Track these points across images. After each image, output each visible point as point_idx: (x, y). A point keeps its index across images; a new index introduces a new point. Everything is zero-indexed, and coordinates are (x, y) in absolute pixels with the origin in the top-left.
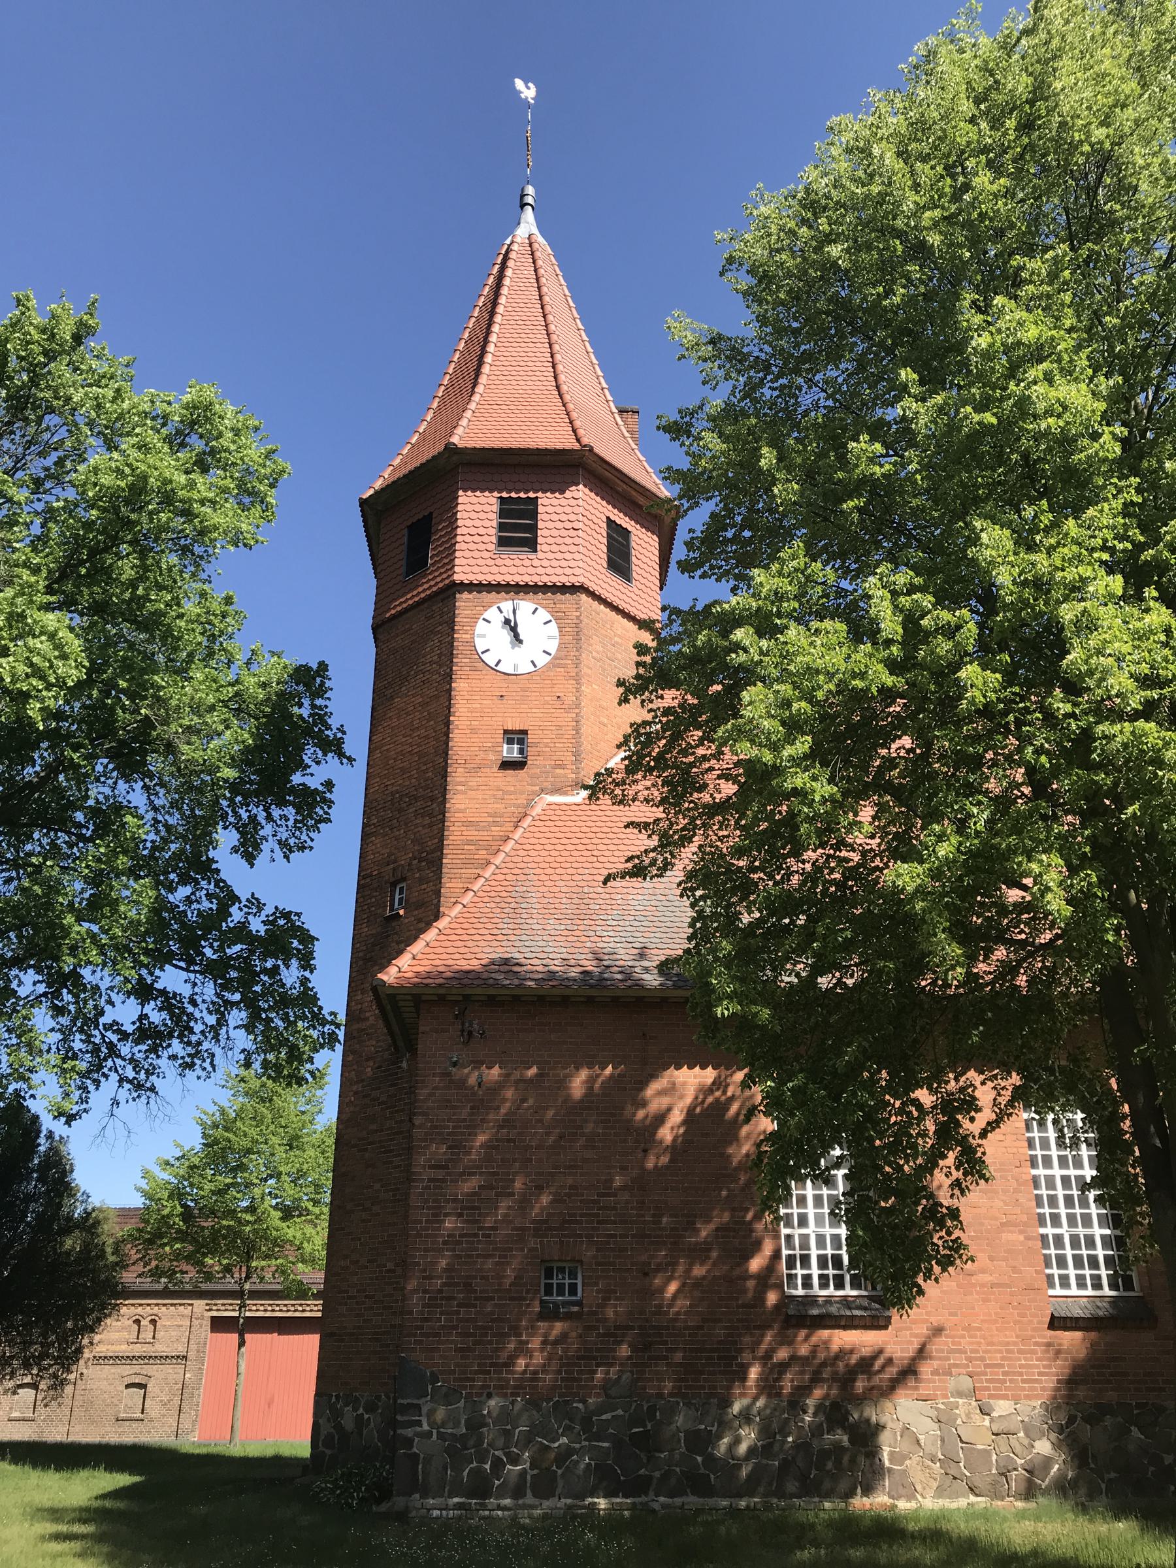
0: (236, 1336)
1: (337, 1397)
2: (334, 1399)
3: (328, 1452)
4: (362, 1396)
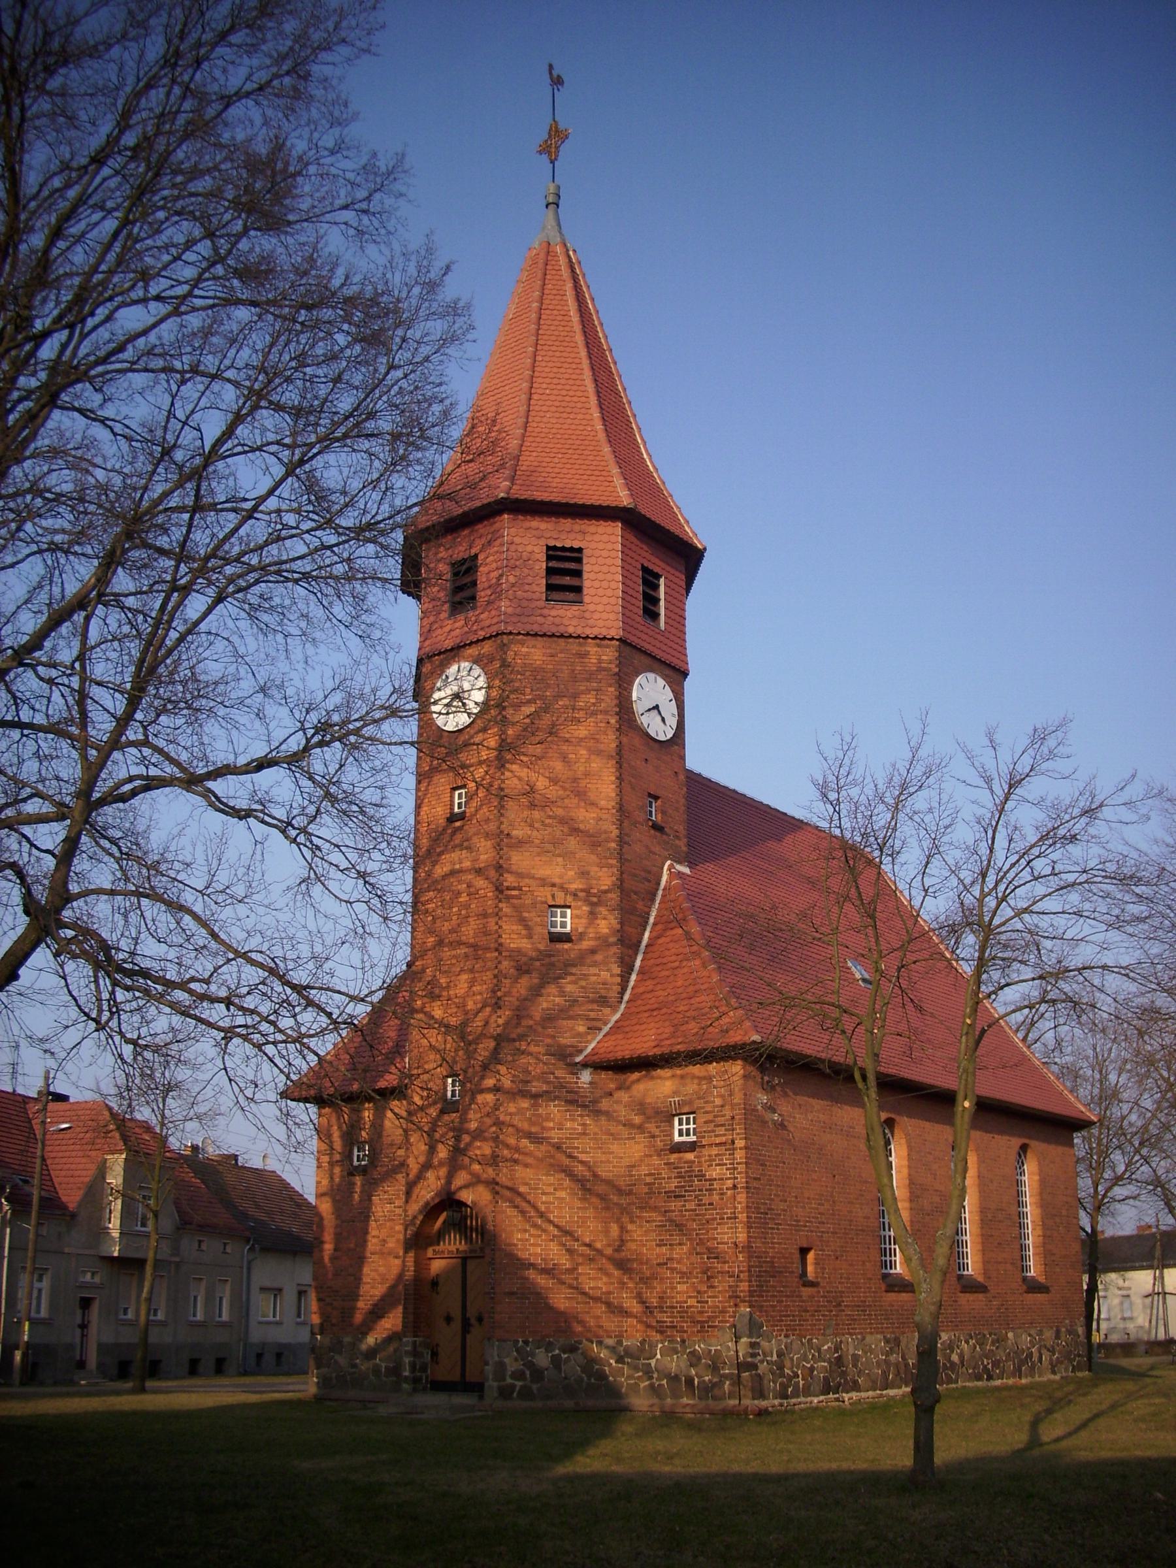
1: (526, 1342)
2: (521, 1343)
3: (519, 1384)
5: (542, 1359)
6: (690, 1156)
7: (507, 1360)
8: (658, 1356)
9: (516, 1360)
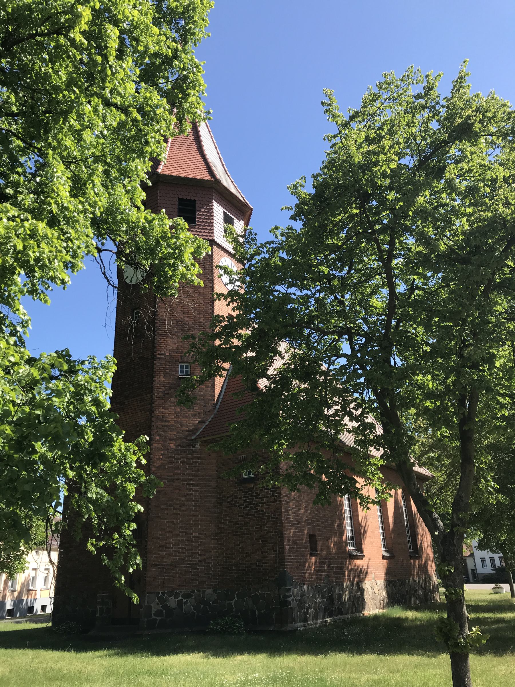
0: (445, 659)
1: (163, 593)
2: (160, 594)
3: (159, 618)
4: (181, 592)
5: (172, 602)
6: (251, 486)
7: (152, 605)
8: (236, 599)
9: (158, 604)
